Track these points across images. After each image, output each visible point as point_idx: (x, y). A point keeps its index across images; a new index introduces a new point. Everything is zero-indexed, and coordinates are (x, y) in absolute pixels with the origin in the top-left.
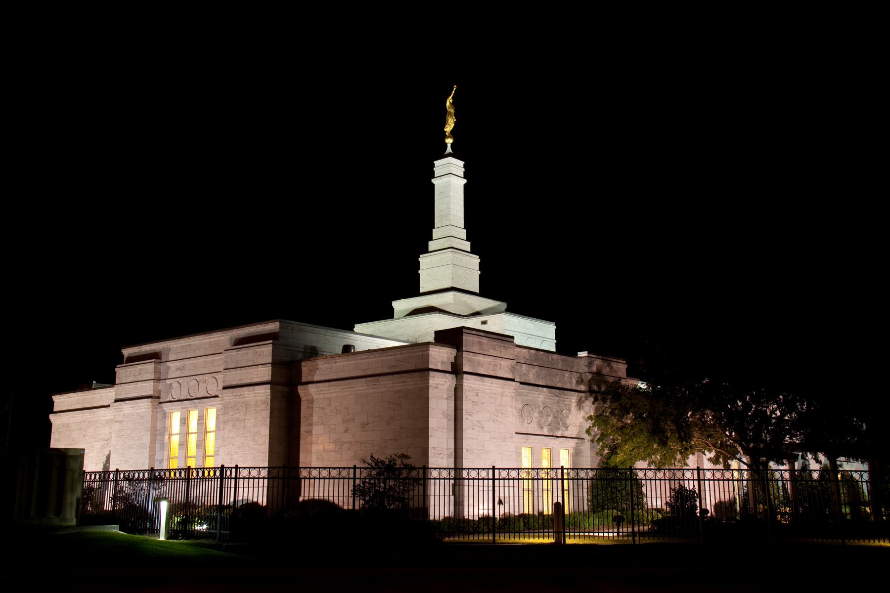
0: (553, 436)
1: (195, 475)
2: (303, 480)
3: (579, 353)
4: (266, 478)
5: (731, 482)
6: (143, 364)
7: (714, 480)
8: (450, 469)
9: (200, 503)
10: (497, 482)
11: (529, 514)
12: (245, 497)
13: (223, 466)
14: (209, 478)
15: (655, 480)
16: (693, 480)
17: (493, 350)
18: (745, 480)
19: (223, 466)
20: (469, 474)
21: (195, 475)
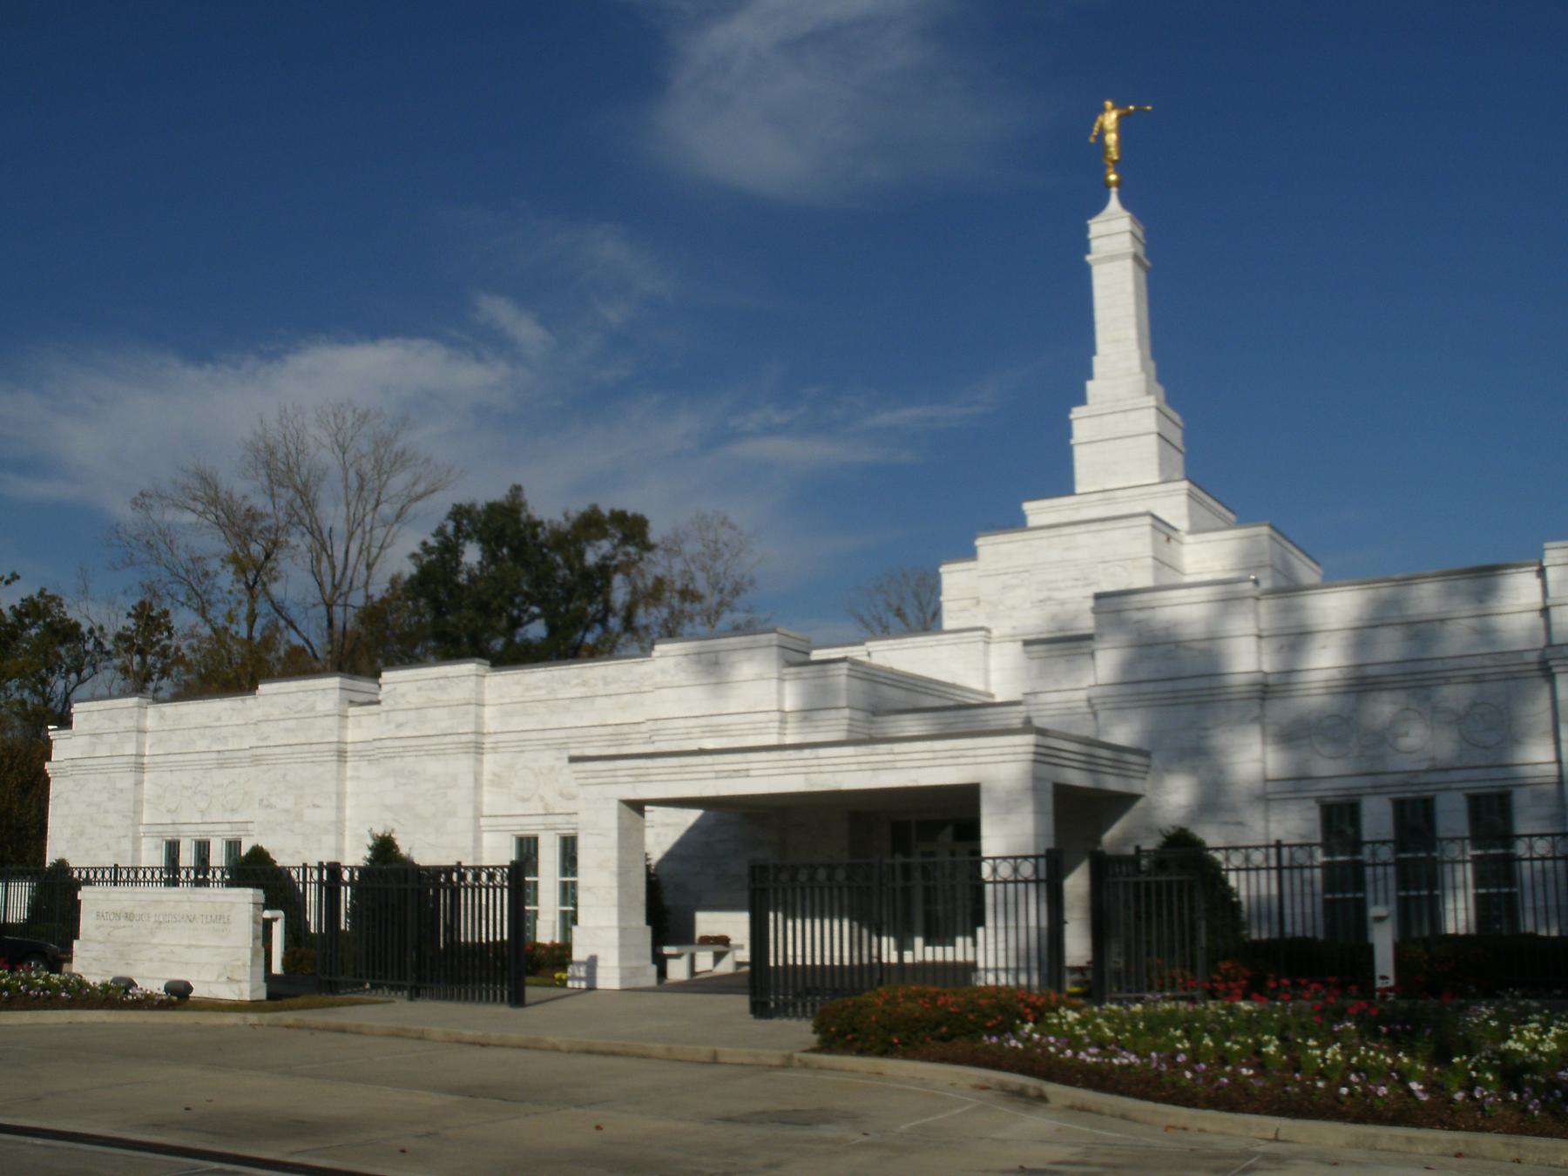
0: (90, 758)
1: (125, 876)
2: (1448, 868)
3: (1029, 507)
4: (1390, 864)
5: (1011, 887)
6: (919, 767)
7: (1016, 882)
8: (1310, 845)
9: (817, 901)
10: (1286, 873)
11: (1007, 986)
12: (1253, 893)
13: (116, 866)
14: (187, 882)
15: (1248, 869)
16: (1268, 868)
17: (897, 619)
18: (1317, 867)
19: (116, 866)
20: (1531, 848)
21: (125, 876)
